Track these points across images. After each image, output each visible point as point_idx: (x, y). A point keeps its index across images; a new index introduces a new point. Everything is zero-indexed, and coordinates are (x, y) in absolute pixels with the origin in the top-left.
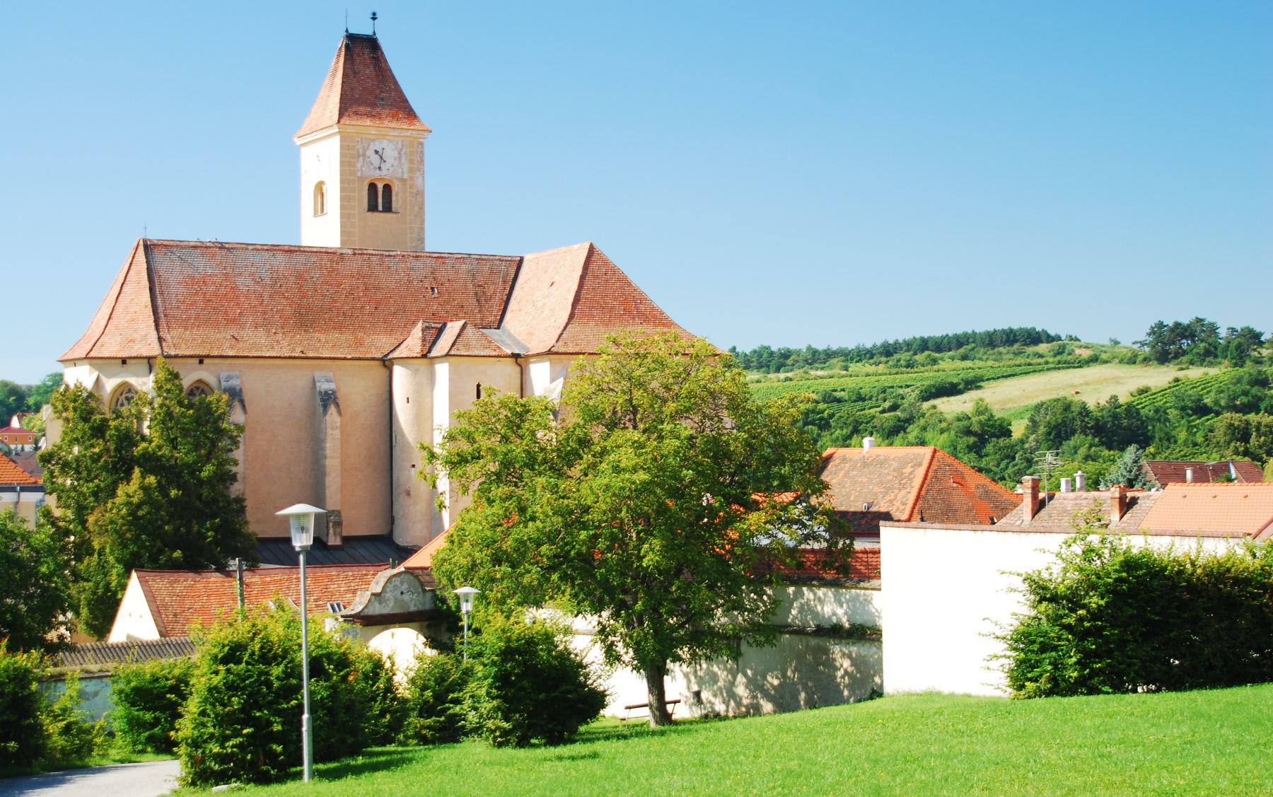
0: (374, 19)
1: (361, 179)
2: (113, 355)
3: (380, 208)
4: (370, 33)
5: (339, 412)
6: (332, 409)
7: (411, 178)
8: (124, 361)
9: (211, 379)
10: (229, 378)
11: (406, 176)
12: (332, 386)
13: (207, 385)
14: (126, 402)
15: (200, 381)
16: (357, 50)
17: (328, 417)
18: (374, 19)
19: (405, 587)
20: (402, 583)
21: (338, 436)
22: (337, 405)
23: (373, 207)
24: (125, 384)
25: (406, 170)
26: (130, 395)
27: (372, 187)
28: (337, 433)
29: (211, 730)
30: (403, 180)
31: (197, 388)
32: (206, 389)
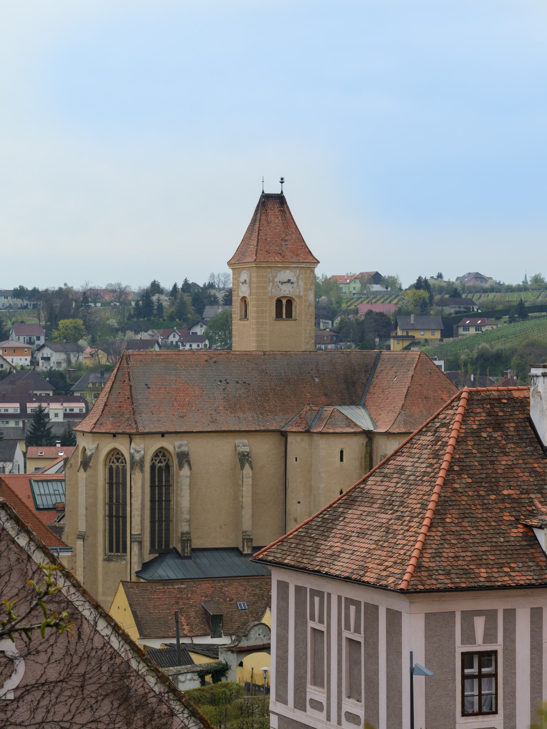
0: (282, 183)
1: (271, 298)
2: (108, 431)
3: (284, 316)
4: (279, 192)
5: (252, 468)
6: (247, 466)
7: (306, 295)
8: (114, 435)
9: (170, 448)
10: (181, 446)
11: (302, 294)
12: (247, 449)
13: (166, 450)
14: (115, 461)
15: (162, 448)
16: (270, 206)
17: (245, 471)
18: (282, 183)
19: (261, 631)
20: (259, 629)
21: (251, 483)
22: (250, 463)
23: (279, 315)
24: (115, 449)
25: (302, 290)
26: (118, 456)
27: (279, 302)
28: (250, 481)
29: (160, 457)
30: (300, 297)
31: (160, 452)
32: (166, 453)
